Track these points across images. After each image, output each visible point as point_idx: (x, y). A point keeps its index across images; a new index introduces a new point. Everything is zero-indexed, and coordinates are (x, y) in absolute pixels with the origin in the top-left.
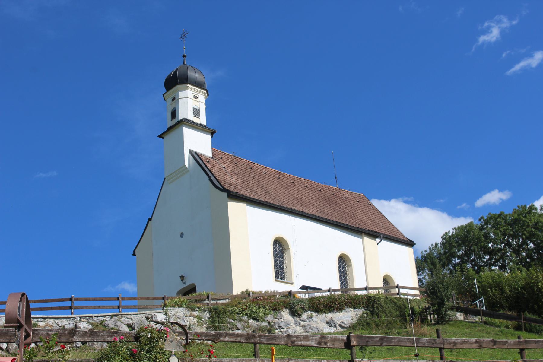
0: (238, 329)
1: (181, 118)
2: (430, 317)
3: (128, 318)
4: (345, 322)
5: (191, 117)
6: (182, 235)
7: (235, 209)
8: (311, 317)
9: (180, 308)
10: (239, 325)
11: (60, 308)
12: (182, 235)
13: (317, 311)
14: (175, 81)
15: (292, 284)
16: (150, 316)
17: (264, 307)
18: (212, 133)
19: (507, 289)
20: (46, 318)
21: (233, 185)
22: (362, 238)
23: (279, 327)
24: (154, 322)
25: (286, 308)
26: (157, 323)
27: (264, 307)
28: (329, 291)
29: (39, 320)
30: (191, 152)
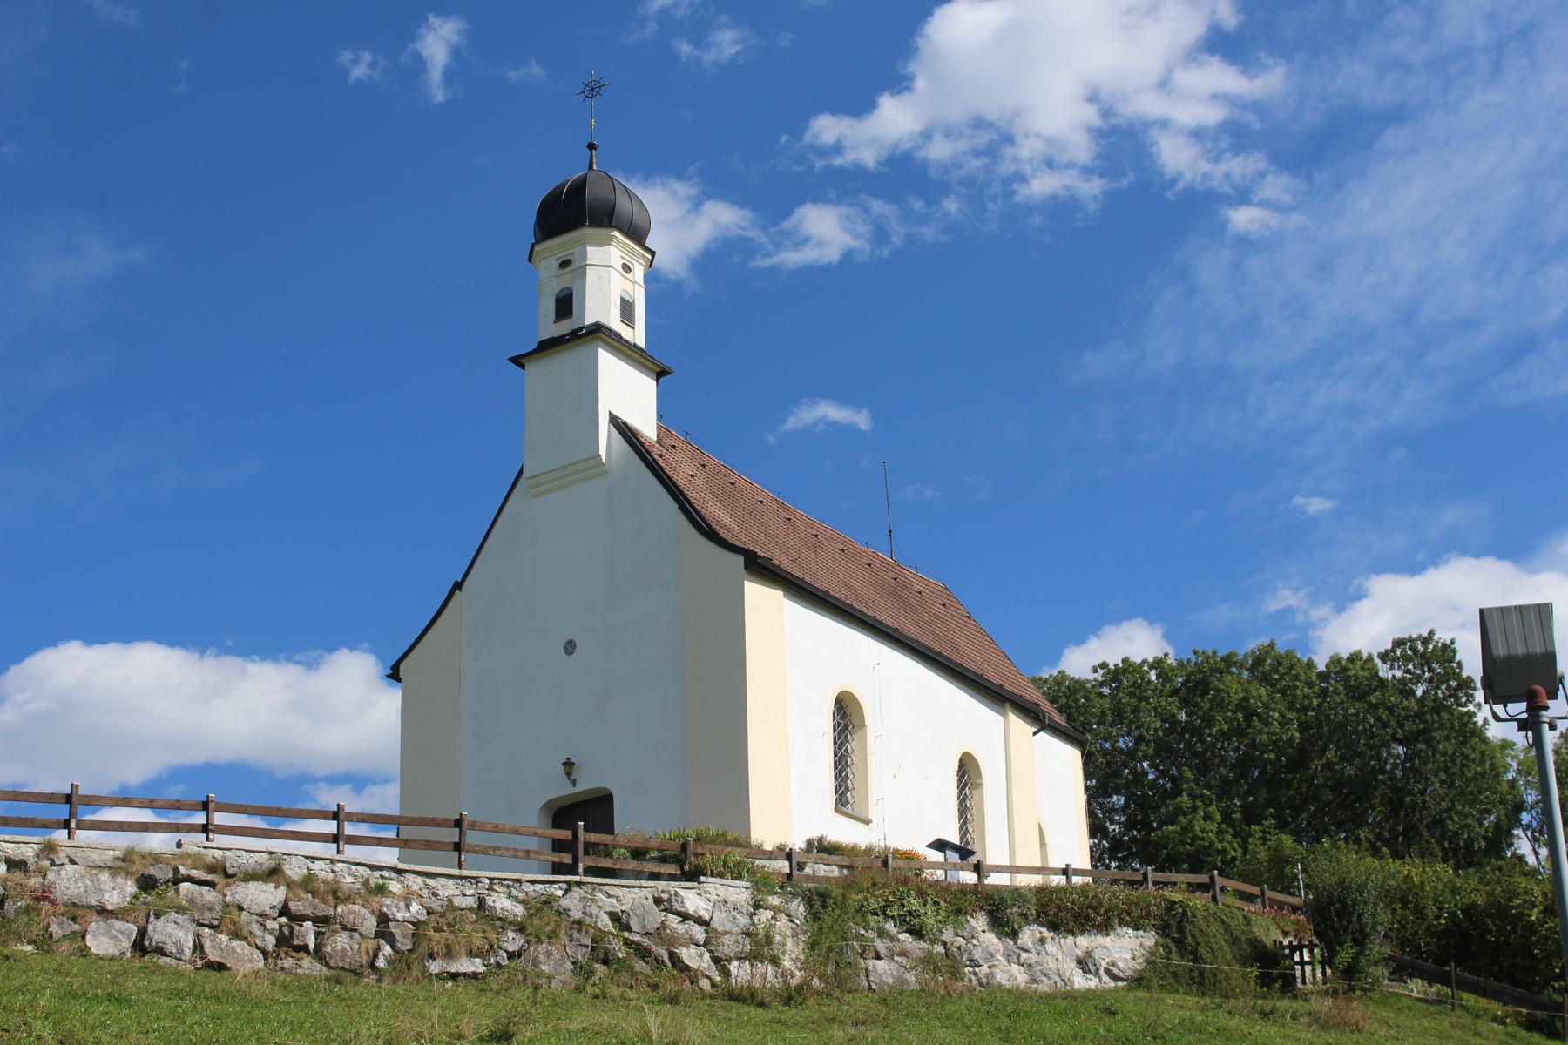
0: (878, 957)
1: (589, 321)
2: (1303, 970)
3: (609, 896)
4: (1121, 965)
5: (615, 323)
6: (570, 647)
7: (760, 599)
8: (1042, 941)
9: (738, 883)
10: (880, 945)
11: (429, 845)
12: (570, 647)
13: (1054, 926)
14: (572, 212)
15: (867, 822)
16: (665, 896)
17: (936, 903)
18: (660, 374)
19: (1431, 910)
20: (405, 871)
21: (729, 530)
22: (1004, 715)
23: (971, 960)
24: (678, 914)
25: (981, 909)
26: (685, 917)
27: (936, 903)
28: (1065, 872)
29: (386, 873)
30: (614, 420)
